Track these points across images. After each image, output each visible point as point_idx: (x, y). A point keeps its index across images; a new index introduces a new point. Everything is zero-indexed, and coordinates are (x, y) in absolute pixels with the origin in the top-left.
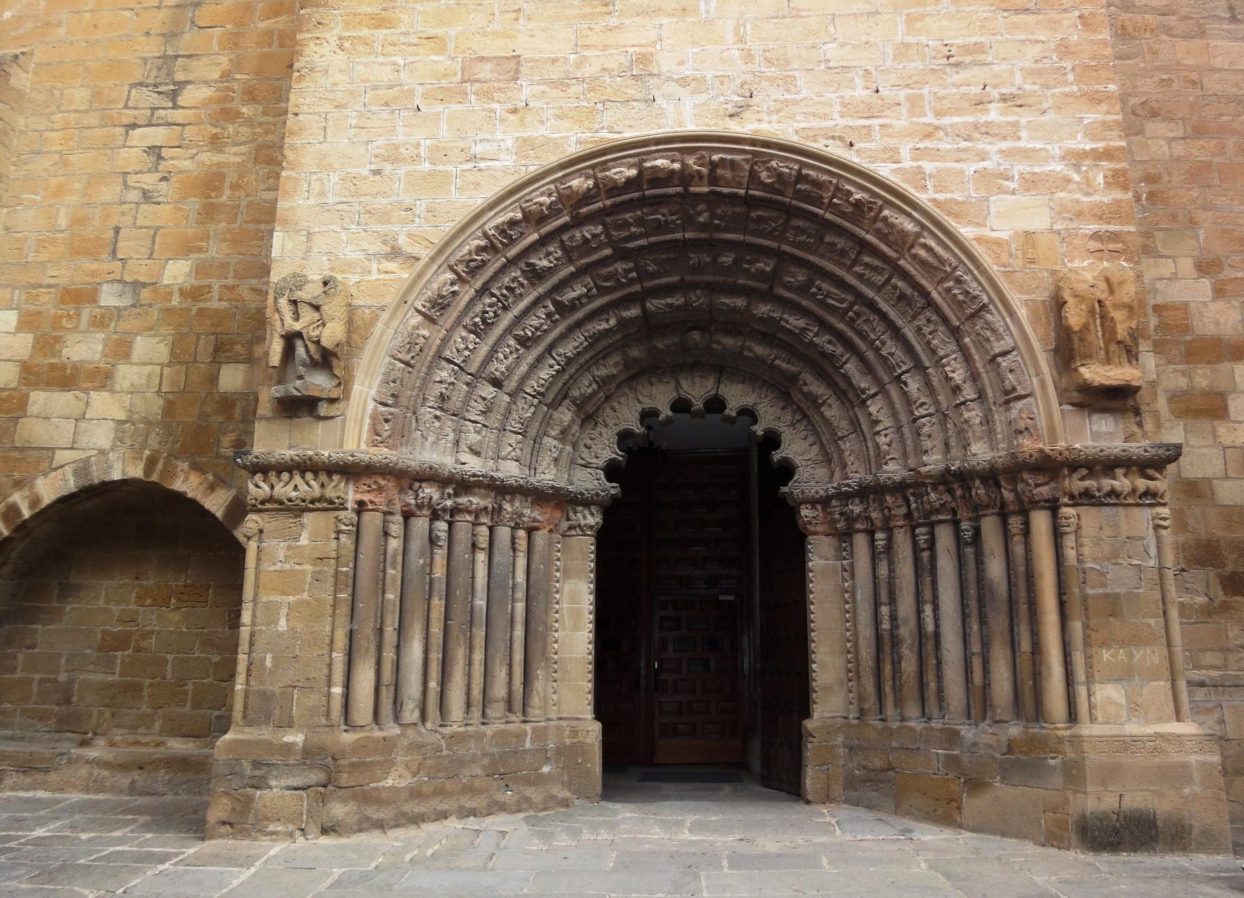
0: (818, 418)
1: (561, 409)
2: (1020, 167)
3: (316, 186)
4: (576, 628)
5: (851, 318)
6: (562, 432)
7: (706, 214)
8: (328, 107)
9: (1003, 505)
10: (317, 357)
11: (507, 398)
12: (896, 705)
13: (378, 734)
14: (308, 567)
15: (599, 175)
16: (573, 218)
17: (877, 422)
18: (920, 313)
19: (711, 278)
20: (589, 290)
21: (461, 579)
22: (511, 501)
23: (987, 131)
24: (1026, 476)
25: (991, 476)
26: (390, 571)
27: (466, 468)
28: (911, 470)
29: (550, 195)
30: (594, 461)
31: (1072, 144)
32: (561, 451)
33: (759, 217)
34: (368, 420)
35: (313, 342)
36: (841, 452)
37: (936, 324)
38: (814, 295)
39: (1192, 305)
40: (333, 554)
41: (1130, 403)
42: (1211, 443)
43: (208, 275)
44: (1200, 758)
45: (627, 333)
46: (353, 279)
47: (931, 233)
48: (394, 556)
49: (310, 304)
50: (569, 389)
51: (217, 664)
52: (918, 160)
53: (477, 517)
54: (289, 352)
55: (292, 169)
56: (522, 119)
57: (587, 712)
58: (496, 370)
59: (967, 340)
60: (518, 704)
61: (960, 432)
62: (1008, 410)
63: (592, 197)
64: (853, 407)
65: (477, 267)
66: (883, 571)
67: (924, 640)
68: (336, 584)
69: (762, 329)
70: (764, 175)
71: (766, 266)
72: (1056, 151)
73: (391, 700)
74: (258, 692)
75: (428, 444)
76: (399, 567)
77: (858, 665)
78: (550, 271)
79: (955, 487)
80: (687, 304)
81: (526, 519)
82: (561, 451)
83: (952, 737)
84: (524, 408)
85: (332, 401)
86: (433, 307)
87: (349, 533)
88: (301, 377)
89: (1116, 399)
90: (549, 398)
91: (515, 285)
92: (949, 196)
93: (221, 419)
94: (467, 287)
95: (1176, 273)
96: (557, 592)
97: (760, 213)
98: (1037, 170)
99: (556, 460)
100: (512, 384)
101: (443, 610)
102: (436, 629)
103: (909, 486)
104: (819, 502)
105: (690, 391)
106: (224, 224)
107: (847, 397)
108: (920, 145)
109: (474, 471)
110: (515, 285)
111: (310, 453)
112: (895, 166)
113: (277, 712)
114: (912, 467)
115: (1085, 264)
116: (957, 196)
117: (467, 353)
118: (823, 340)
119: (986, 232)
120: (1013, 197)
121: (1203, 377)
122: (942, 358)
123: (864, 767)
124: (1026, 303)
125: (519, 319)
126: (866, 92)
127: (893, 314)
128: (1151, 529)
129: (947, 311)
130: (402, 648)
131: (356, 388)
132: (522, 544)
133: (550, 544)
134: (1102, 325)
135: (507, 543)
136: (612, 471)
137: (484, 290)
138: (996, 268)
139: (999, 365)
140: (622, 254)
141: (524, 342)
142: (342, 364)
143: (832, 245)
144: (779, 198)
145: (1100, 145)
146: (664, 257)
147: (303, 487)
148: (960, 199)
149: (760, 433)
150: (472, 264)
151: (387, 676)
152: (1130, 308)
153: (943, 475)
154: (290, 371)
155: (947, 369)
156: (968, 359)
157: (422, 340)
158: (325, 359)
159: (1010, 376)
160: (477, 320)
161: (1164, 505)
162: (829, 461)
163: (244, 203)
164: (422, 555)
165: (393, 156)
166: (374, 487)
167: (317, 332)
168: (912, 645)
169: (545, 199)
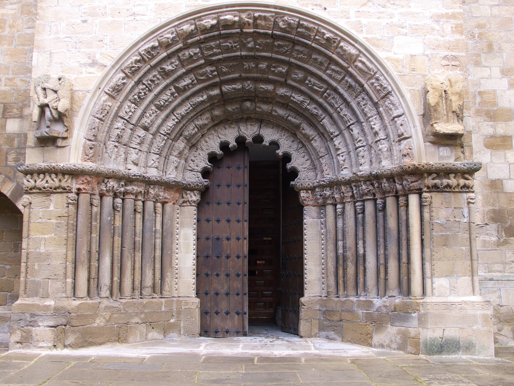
0: (310, 147)
1: (179, 141)
5: (325, 96)
6: (179, 153)
7: (252, 43)
9: (397, 192)
10: (56, 116)
11: (151, 136)
12: (344, 290)
13: (90, 301)
14: (54, 221)
15: (198, 23)
16: (184, 45)
17: (338, 149)
18: (359, 95)
19: (255, 75)
20: (193, 81)
22: (153, 189)
24: (406, 177)
25: (391, 177)
26: (94, 223)
27: (131, 171)
28: (354, 174)
29: (172, 33)
30: (196, 168)
32: (179, 163)
33: (279, 45)
35: (54, 109)
37: (367, 101)
38: (307, 84)
39: (498, 92)
41: (459, 142)
42: (503, 161)
45: (212, 103)
46: (73, 77)
50: (183, 131)
51: (9, 269)
52: (359, 17)
54: (42, 113)
55: (42, 20)
57: (193, 294)
59: (381, 109)
60: (158, 289)
63: (194, 34)
65: (135, 70)
67: (358, 258)
70: (281, 24)
71: (283, 69)
74: (32, 281)
76: (98, 221)
77: (327, 270)
78: (173, 72)
79: (375, 182)
80: (243, 88)
81: (161, 198)
83: (369, 304)
84: (159, 142)
85: (64, 138)
86: (113, 91)
87: (73, 204)
89: (451, 140)
90: (173, 136)
91: (155, 79)
92: (374, 36)
93: (7, 147)
95: (491, 75)
96: (177, 234)
97: (280, 43)
99: (176, 167)
100: (153, 129)
102: (117, 252)
103: (353, 182)
104: (310, 190)
105: (245, 132)
106: (6, 46)
108: (360, 10)
110: (155, 79)
111: (54, 164)
113: (41, 290)
115: (440, 72)
116: (378, 36)
119: (391, 55)
121: (501, 129)
122: (369, 118)
125: (157, 96)
127: (346, 95)
131: (75, 132)
133: (173, 210)
134: (446, 103)
135: (152, 209)
136: (205, 173)
137: (139, 82)
138: (395, 73)
142: (69, 119)
143: (316, 59)
144: (289, 35)
145: (450, 11)
146: (231, 64)
147: (51, 181)
148: (380, 38)
149: (281, 154)
150: (133, 69)
152: (460, 95)
153: (369, 176)
154: (43, 123)
155: (372, 123)
156: (382, 118)
157: (108, 108)
158: (60, 118)
159: (401, 127)
160: (136, 97)
161: (473, 192)
162: (316, 168)
163: (16, 35)
166: (85, 181)
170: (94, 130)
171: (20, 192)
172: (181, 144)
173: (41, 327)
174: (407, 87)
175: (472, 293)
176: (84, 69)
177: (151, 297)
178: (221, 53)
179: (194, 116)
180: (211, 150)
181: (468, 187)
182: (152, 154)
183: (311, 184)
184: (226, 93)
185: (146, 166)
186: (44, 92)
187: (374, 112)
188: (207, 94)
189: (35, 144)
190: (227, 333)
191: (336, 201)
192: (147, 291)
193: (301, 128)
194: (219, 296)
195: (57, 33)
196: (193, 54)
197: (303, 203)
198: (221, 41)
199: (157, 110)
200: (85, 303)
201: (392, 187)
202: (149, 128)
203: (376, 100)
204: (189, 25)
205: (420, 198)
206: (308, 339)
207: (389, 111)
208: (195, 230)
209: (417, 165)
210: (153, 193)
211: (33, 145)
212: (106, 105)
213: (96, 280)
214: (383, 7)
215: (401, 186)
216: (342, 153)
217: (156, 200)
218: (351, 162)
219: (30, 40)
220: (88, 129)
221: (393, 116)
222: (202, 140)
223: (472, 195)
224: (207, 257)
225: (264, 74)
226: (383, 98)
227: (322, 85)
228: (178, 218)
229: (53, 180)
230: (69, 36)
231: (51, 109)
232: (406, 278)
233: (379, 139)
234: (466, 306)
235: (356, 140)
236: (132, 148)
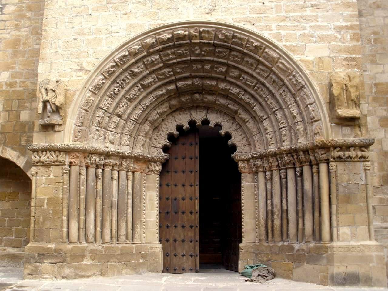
1: (145, 125)
2: (318, 33)
3: (54, 45)
4: (152, 209)
5: (256, 89)
6: (145, 134)
7: (199, 50)
8: (57, 15)
9: (311, 162)
10: (54, 109)
11: (124, 122)
13: (79, 245)
15: (157, 37)
17: (267, 129)
18: (281, 88)
19: (201, 74)
20: (154, 80)
21: (107, 191)
22: (126, 161)
23: (305, 18)
25: (306, 151)
26: (82, 188)
27: (108, 149)
28: (279, 148)
30: (158, 145)
32: (145, 141)
33: (219, 51)
34: (73, 132)
37: (287, 92)
38: (242, 80)
40: (61, 181)
41: (357, 123)
43: (15, 78)
44: (377, 253)
45: (170, 96)
47: (284, 58)
48: (83, 182)
49: (52, 90)
50: (148, 117)
52: (279, 30)
53: (113, 167)
54: (45, 107)
55: (45, 39)
56: (128, 17)
57: (157, 241)
58: (119, 111)
60: (130, 237)
61: (296, 134)
62: (312, 125)
63: (155, 45)
65: (112, 73)
66: (269, 187)
68: (63, 192)
69: (223, 93)
70: (220, 36)
71: (223, 69)
72: (332, 26)
73: (84, 234)
75: (94, 140)
76: (85, 186)
81: (131, 168)
82: (145, 141)
84: (130, 126)
85: (60, 125)
86: (95, 89)
87: (67, 173)
88: (49, 117)
89: (351, 122)
90: (140, 121)
92: (290, 43)
94: (108, 81)
95: (384, 71)
96: (144, 196)
98: (324, 33)
99: (143, 145)
100: (125, 116)
101: (101, 202)
102: (99, 209)
104: (246, 160)
105: (195, 117)
106: (20, 59)
108: (280, 24)
111: (53, 144)
114: (279, 147)
115: (342, 70)
116: (294, 44)
117: (108, 105)
118: (246, 97)
119: (304, 58)
120: (315, 44)
122: (289, 105)
124: (319, 85)
126: (259, 4)
127: (271, 88)
128: (363, 170)
131: (68, 120)
132: (130, 177)
134: (346, 94)
135: (125, 177)
136: (165, 149)
138: (308, 71)
139: (309, 108)
140: (167, 66)
141: (130, 100)
142: (63, 111)
143: (247, 61)
144: (226, 44)
145: (349, 24)
146: (183, 66)
148: (295, 45)
149: (223, 133)
151: (82, 226)
152: (357, 87)
153: (290, 150)
154: (45, 114)
155: (291, 109)
156: (298, 106)
158: (57, 110)
159: (312, 112)
160: (112, 93)
161: (368, 161)
162: (250, 144)
163: (28, 50)
164: (93, 182)
165: (81, 33)
166: (75, 156)
167: (54, 100)
168: (279, 215)
169: (137, 47)
170: (81, 118)
171: (29, 164)
173: (46, 264)
174: (317, 82)
175: (368, 239)
176: (74, 74)
177: (125, 243)
178: (176, 58)
179: (156, 105)
180: (170, 131)
181: (365, 158)
182: (124, 135)
183: (247, 157)
184: (180, 88)
185: (120, 144)
186: (46, 91)
187: (293, 101)
188: (165, 89)
189: (40, 129)
190: (183, 270)
191: (265, 169)
193: (238, 114)
194: (177, 243)
195: (56, 48)
196: (154, 60)
197: (241, 171)
198: (175, 49)
199: (128, 102)
200: (76, 246)
201: (307, 158)
202: (122, 115)
204: (151, 39)
205: (328, 166)
207: (304, 100)
208: (157, 192)
209: (325, 141)
210: (125, 164)
211: (39, 131)
212: (90, 100)
213: (84, 230)
214: (297, 22)
215: (314, 157)
217: (128, 170)
218: (277, 139)
219: (37, 53)
220: (77, 118)
221: (306, 104)
222: (163, 123)
223: (368, 164)
224: (167, 213)
225: (209, 73)
226: (299, 90)
227: (253, 81)
228: (145, 183)
230: (64, 50)
231: (51, 104)
232: (318, 227)
233: (297, 121)
234: (364, 249)
235: (280, 122)
236: (110, 131)
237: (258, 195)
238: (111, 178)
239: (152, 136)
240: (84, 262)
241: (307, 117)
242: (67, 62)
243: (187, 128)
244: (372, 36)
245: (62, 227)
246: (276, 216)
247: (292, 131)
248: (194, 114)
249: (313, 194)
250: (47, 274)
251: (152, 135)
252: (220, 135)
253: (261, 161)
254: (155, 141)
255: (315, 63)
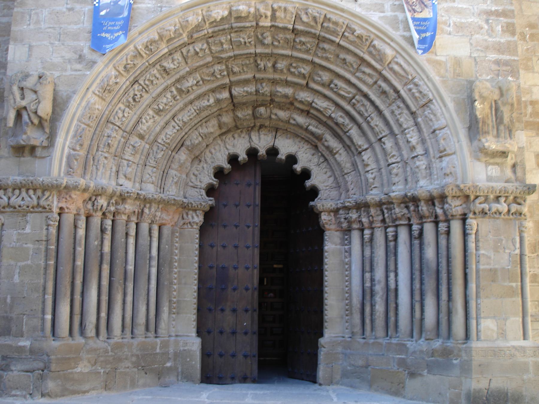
3: (34, 17)
9: (436, 217)
13: (70, 341)
14: (30, 245)
17: (367, 165)
18: (393, 102)
20: (198, 82)
21: (120, 253)
27: (123, 188)
28: (386, 194)
31: (484, 7)
34: (64, 159)
36: (346, 182)
49: (32, 90)
52: (395, 12)
57: (193, 333)
61: (414, 173)
62: (441, 161)
64: (354, 156)
66: (367, 253)
71: (305, 69)
83: (402, 348)
98: (463, 21)
102: (105, 282)
103: (384, 204)
107: (351, 150)
109: (127, 190)
111: (31, 178)
112: (382, 15)
120: (449, 36)
122: (405, 130)
123: (353, 365)
125: (155, 99)
127: (378, 102)
129: (409, 102)
130: (85, 294)
136: (210, 191)
138: (437, 78)
141: (159, 112)
145: (500, 8)
153: (404, 198)
155: (408, 136)
156: (420, 130)
162: (339, 187)
168: (383, 295)
172: (183, 156)
173: (15, 372)
175: (522, 338)
183: (334, 206)
186: (20, 92)
187: (411, 123)
191: (363, 225)
192: (140, 330)
193: (324, 140)
197: (324, 227)
203: (414, 109)
206: (328, 387)
216: (372, 170)
218: (382, 180)
221: (433, 128)
222: (207, 151)
229: (30, 197)
230: (52, 26)
231: (30, 113)
232: (446, 318)
233: (416, 154)
237: (350, 264)
238: (124, 234)
239: (190, 170)
240: (79, 370)
241: (433, 148)
242: (56, 46)
243: (281, 159)
244: (527, 29)
245: (43, 312)
246: (379, 298)
247: (408, 169)
248: (254, 136)
249: (438, 265)
250: (17, 389)
251: (189, 168)
252: (293, 171)
253: (357, 212)
254: (194, 177)
255: (449, 65)
